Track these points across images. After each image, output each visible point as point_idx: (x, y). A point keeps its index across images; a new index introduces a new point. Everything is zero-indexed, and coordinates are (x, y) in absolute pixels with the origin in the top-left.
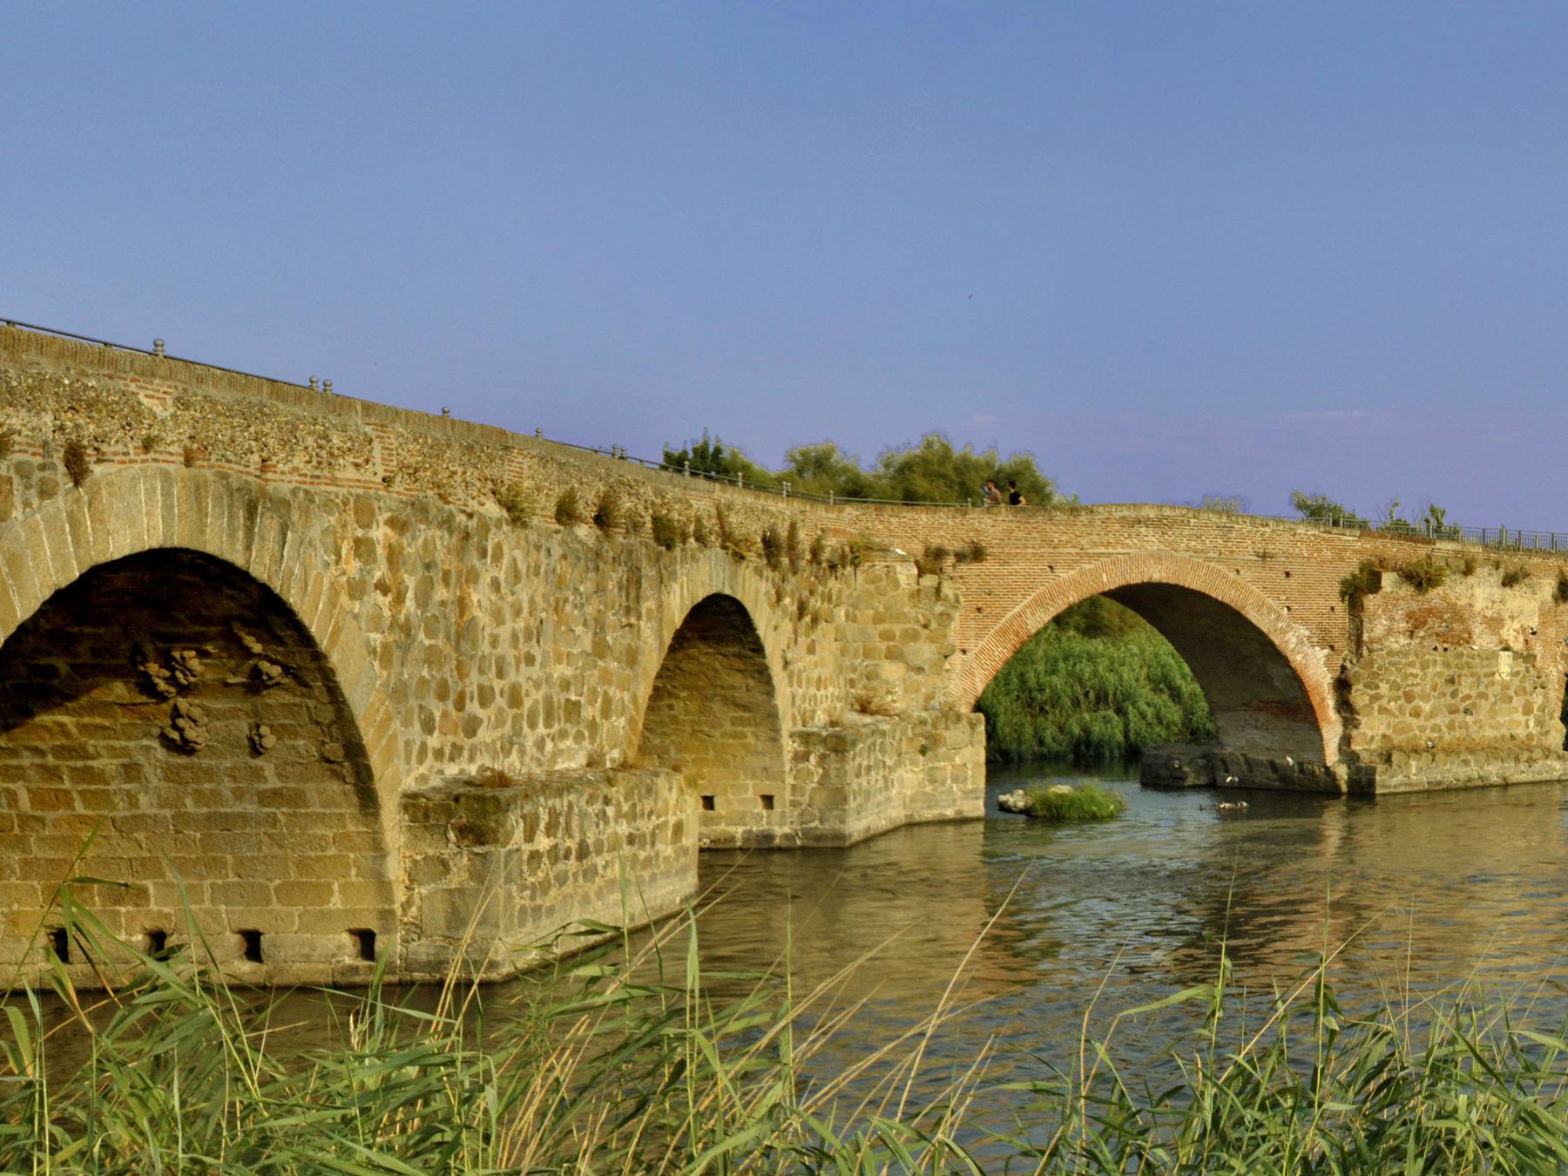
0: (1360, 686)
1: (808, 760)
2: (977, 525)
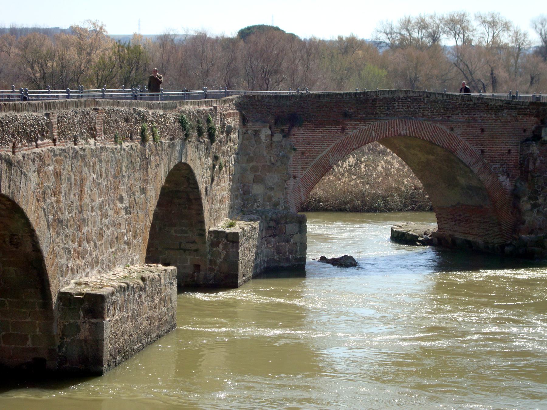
0: (525, 199)
1: (219, 247)
2: (303, 104)
